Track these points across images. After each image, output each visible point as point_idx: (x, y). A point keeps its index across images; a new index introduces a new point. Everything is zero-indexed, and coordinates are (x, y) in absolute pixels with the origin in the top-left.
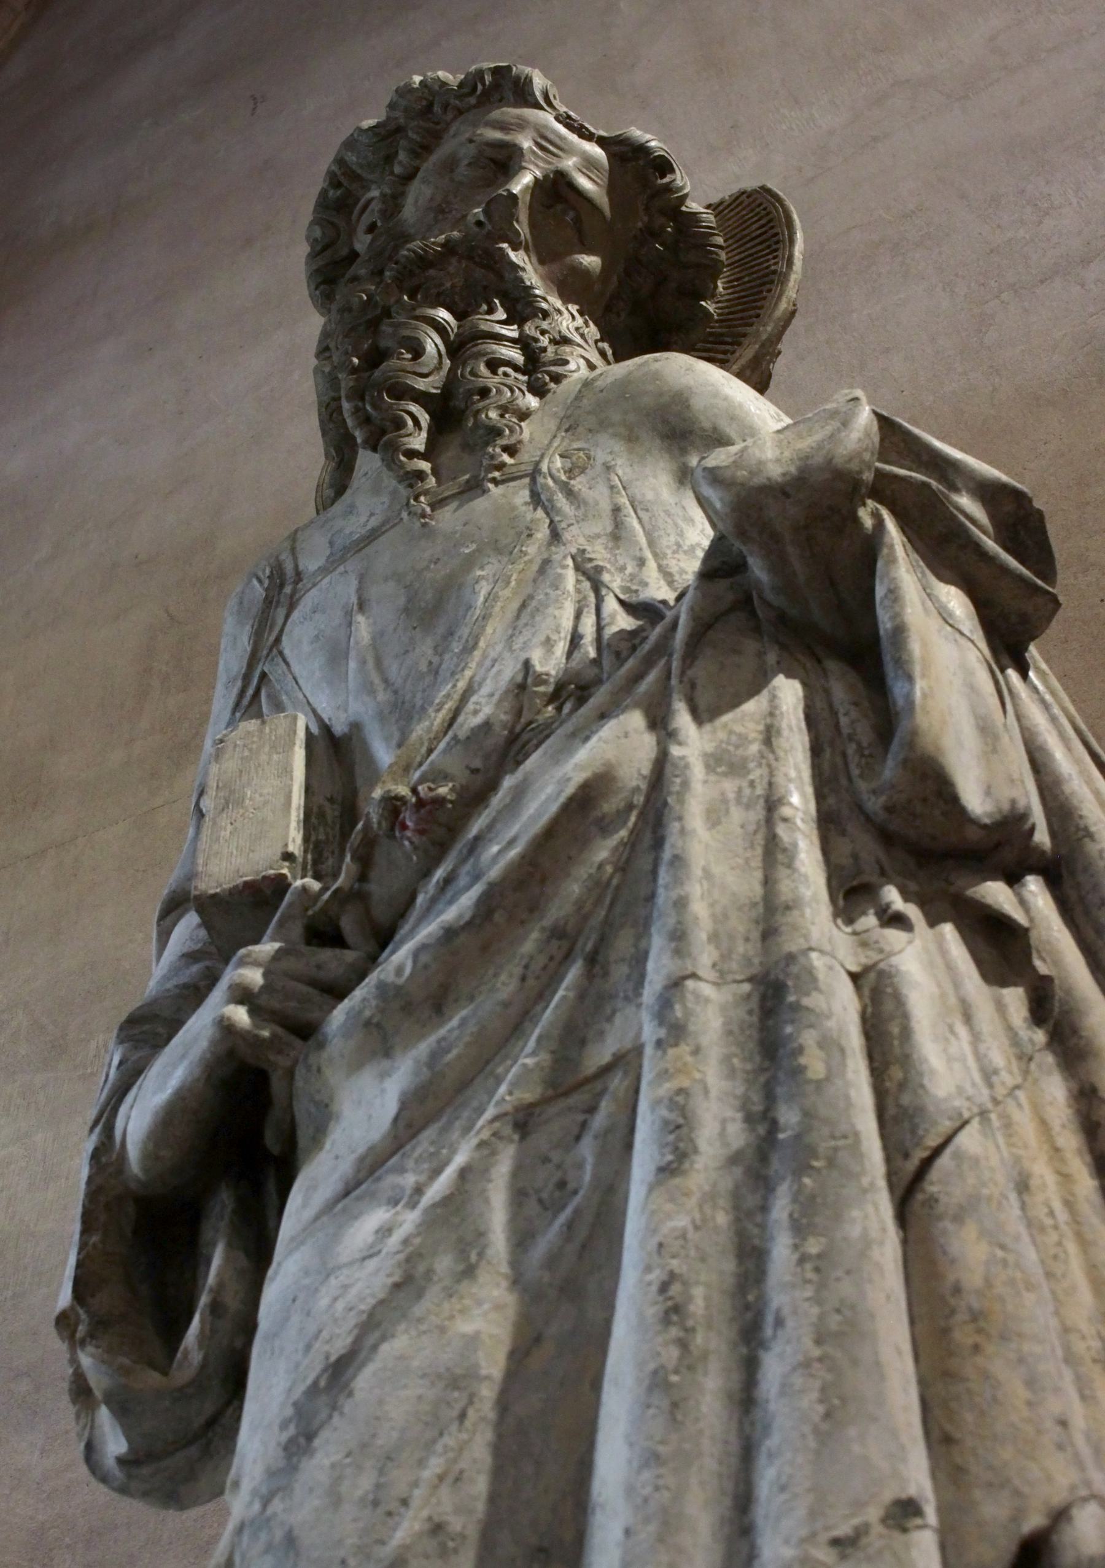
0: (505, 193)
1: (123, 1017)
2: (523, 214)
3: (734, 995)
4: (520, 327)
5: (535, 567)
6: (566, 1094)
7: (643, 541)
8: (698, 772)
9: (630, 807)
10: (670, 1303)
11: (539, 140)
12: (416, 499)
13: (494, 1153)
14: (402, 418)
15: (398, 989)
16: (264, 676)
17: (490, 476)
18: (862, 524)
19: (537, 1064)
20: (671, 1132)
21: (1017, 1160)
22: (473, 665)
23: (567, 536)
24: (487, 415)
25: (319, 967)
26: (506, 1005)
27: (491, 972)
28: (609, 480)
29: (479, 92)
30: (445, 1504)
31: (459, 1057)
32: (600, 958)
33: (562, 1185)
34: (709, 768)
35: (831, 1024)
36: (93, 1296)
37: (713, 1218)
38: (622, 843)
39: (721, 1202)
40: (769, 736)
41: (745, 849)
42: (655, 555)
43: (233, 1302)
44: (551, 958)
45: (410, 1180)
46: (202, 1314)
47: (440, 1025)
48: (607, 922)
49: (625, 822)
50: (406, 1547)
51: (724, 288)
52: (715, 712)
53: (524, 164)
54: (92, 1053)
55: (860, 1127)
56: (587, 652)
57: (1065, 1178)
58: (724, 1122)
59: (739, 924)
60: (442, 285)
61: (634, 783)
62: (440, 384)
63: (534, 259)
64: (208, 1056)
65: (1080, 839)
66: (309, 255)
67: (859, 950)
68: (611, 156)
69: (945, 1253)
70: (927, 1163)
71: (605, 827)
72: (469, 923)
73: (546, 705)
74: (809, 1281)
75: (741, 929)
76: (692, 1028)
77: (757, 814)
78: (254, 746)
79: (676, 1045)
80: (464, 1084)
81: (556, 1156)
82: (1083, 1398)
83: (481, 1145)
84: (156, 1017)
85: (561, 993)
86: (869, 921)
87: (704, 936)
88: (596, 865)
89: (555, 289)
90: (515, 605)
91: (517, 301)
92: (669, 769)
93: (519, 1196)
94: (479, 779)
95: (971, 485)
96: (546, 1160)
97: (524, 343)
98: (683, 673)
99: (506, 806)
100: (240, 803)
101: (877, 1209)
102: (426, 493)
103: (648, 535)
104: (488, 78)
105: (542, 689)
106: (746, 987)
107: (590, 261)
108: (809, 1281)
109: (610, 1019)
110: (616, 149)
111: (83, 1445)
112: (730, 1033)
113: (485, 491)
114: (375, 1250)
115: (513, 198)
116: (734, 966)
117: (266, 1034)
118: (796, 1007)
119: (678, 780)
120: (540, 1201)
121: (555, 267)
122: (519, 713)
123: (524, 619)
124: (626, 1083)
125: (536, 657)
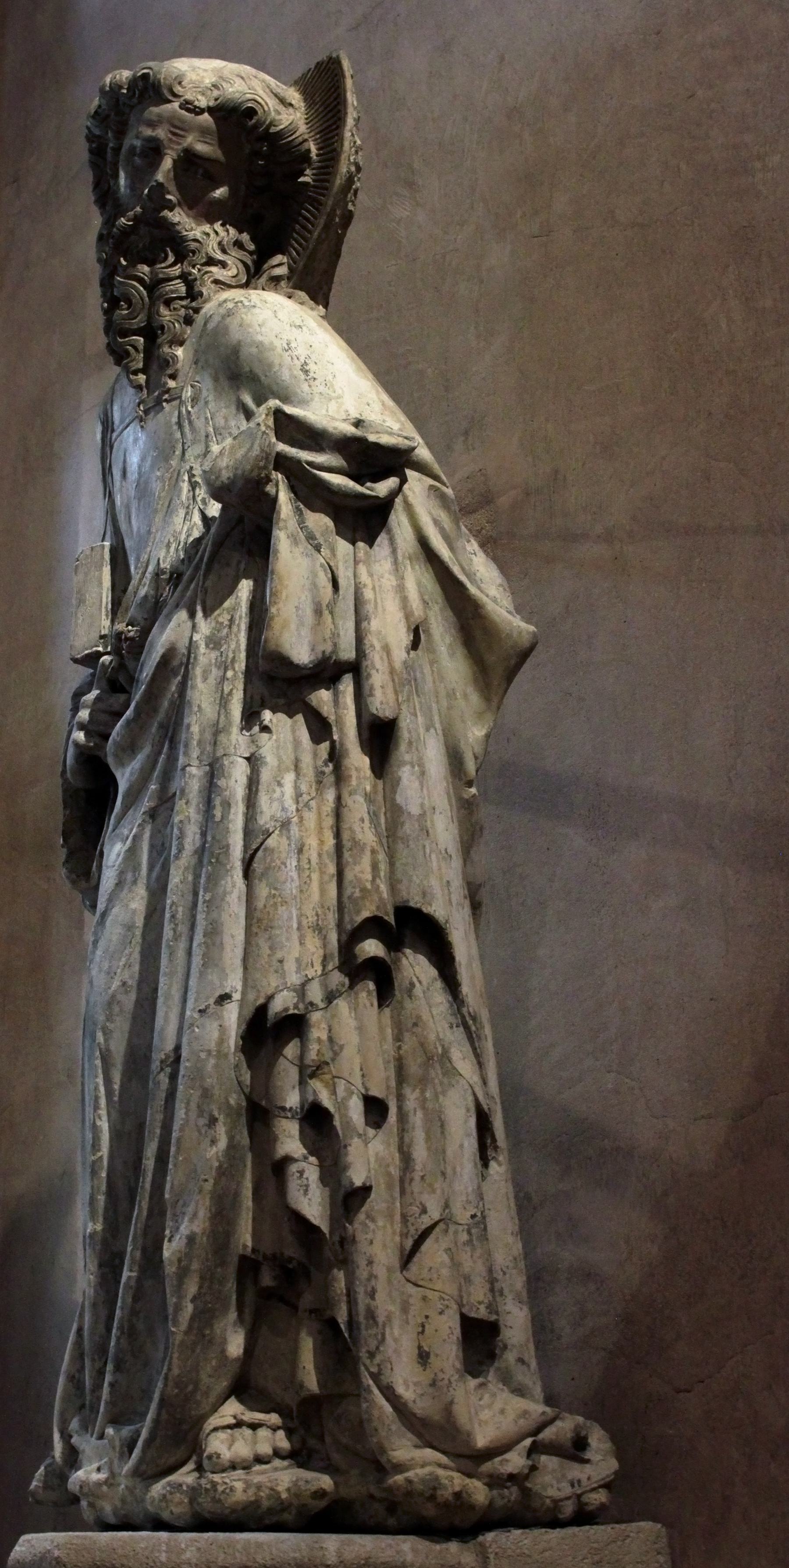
0: (154, 184)
1: (71, 695)
2: (172, 187)
4: (182, 265)
8: (202, 649)
9: (181, 664)
11: (172, 129)
13: (143, 829)
21: (301, 837)
22: (150, 544)
23: (187, 456)
25: (111, 706)
30: (126, 975)
33: (163, 844)
34: (207, 646)
35: (227, 793)
39: (191, 871)
50: (115, 991)
51: (317, 155)
52: (213, 610)
57: (322, 842)
58: (195, 834)
59: (208, 736)
62: (145, 318)
63: (186, 208)
76: (187, 791)
82: (301, 944)
86: (256, 729)
87: (195, 743)
89: (203, 219)
93: (152, 847)
97: (184, 277)
98: (204, 583)
104: (140, 84)
106: (208, 768)
107: (220, 192)
113: (163, 408)
115: (160, 185)
117: (92, 744)
125: (162, 554)
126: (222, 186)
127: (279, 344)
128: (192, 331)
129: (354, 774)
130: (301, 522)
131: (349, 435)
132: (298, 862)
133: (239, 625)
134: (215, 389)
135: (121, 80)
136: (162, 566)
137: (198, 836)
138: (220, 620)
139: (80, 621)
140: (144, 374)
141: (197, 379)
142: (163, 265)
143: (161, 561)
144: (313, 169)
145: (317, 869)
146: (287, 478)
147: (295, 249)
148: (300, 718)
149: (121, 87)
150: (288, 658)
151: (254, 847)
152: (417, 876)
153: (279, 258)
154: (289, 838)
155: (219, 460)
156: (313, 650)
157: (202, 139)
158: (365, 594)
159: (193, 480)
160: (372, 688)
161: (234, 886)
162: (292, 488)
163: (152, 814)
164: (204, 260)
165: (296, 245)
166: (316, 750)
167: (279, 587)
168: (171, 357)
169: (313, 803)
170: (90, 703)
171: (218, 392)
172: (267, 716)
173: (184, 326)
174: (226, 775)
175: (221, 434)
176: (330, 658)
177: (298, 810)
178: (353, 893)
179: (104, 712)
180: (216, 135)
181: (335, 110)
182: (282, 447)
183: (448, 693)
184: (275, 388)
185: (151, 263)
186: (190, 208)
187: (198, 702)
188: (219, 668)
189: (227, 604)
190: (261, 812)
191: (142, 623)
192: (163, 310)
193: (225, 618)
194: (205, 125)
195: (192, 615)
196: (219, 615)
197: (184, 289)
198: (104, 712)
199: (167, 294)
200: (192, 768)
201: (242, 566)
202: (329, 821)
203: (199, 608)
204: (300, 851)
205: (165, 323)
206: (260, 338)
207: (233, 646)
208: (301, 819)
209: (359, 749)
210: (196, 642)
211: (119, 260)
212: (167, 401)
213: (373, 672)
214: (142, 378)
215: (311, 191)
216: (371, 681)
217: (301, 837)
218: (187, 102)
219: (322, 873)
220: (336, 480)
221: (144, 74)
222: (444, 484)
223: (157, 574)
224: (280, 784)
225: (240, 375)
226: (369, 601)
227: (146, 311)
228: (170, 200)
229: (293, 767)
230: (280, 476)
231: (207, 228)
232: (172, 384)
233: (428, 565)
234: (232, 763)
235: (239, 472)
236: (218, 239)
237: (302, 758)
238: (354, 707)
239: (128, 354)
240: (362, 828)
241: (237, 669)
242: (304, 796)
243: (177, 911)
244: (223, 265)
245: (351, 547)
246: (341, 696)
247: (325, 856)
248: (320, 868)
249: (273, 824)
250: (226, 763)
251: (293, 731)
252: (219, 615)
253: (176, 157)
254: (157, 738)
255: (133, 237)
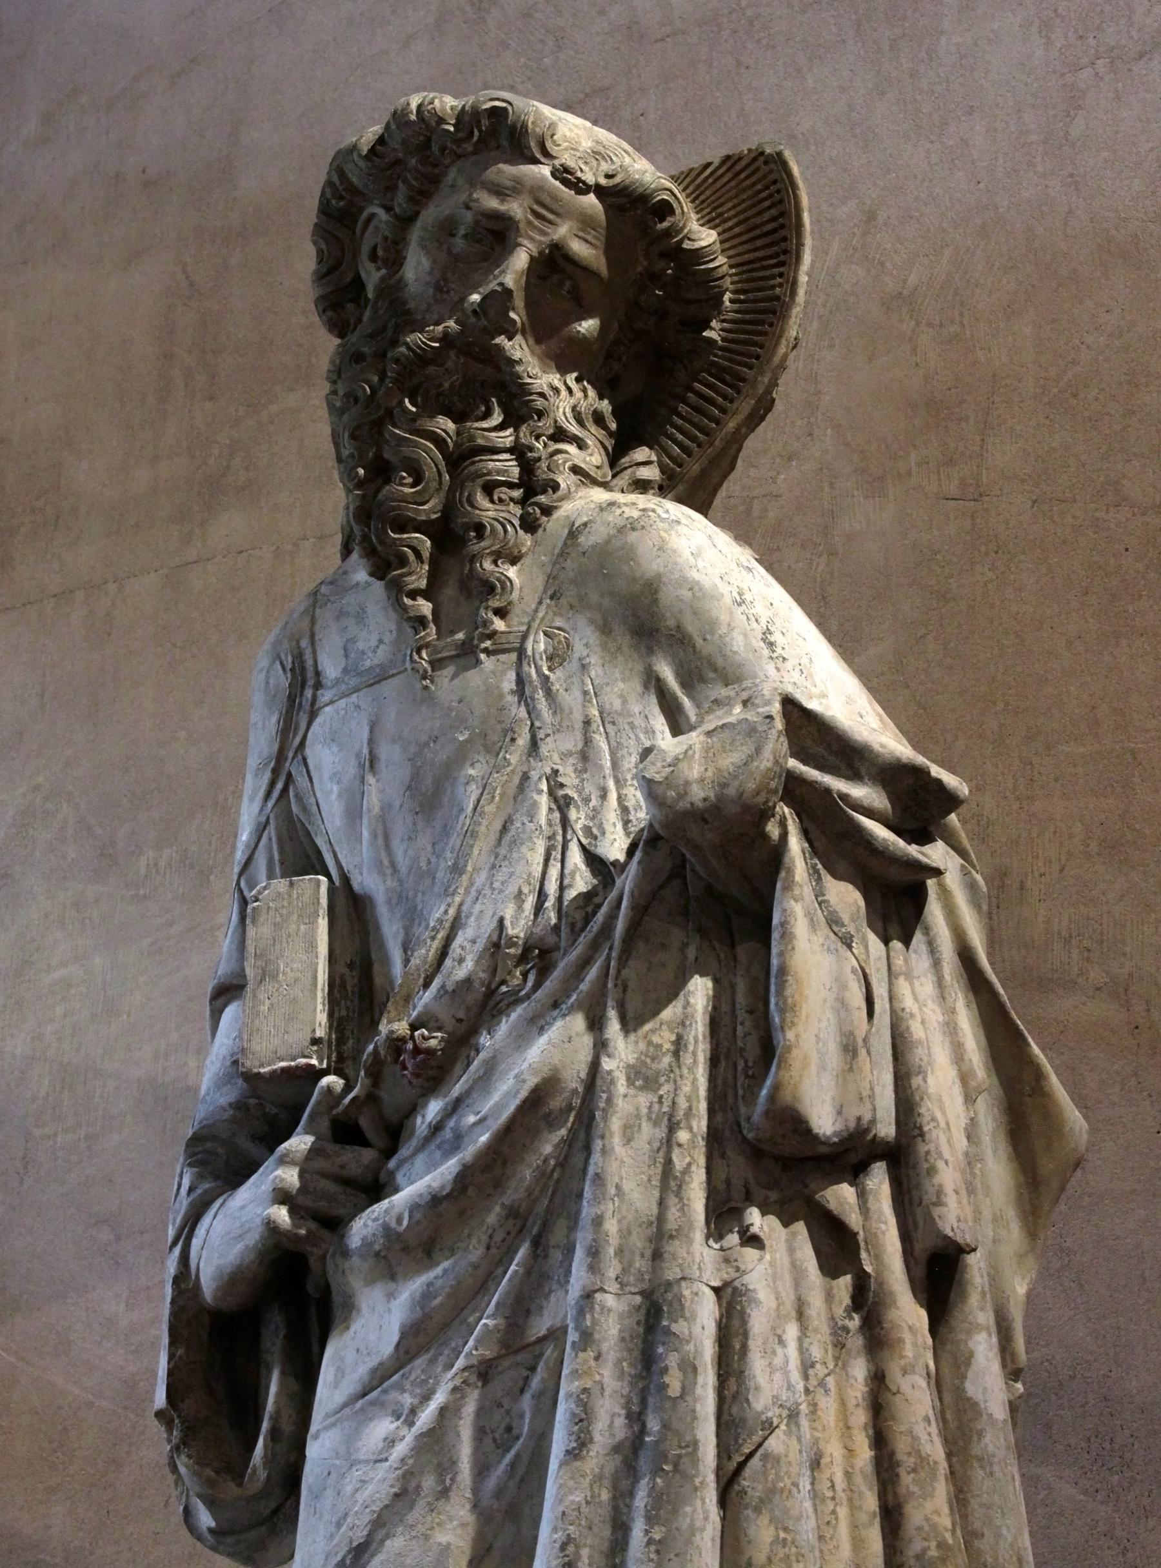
0: (499, 289)
2: (519, 301)
3: (629, 1304)
4: (516, 430)
5: (516, 780)
6: (517, 1352)
7: (608, 770)
8: (621, 1086)
9: (570, 1108)
10: (567, 1559)
11: (535, 207)
12: (419, 652)
13: (463, 1397)
14: (405, 553)
15: (399, 1236)
16: (289, 776)
17: (483, 645)
18: (770, 838)
19: (495, 1326)
20: (577, 1424)
21: (817, 1441)
22: (461, 891)
23: (544, 749)
24: (481, 566)
25: (343, 1167)
26: (476, 1267)
27: (466, 1232)
28: (583, 683)
29: (475, 139)
31: (441, 1305)
32: (543, 1241)
33: (509, 1429)
34: (630, 1082)
35: (690, 1348)
36: (183, 1401)
37: (599, 1495)
38: (563, 1140)
39: (606, 1483)
40: (679, 1045)
41: (649, 1166)
42: (617, 781)
43: (287, 1427)
44: (509, 1233)
45: (408, 1400)
46: (265, 1440)
47: (429, 1267)
48: (549, 1211)
49: (566, 1121)
52: (641, 1021)
53: (520, 240)
54: (143, 871)
55: (700, 1435)
56: (550, 919)
57: (850, 1452)
58: (613, 1415)
59: (638, 1241)
60: (441, 385)
61: (574, 1085)
62: (440, 507)
63: (531, 341)
64: (260, 1246)
65: (914, 1137)
66: (316, 272)
67: (723, 1266)
68: (608, 208)
69: (746, 1535)
70: (742, 1465)
71: (552, 1121)
72: (448, 1195)
73: (516, 967)
74: (651, 1560)
75: (639, 1245)
76: (597, 1336)
77: (661, 1133)
78: (284, 911)
79: (585, 1350)
80: (445, 1326)
81: (506, 1402)
83: (455, 1389)
84: (214, 1138)
85: (513, 1267)
86: (733, 1239)
87: (611, 1251)
88: (542, 1158)
90: (497, 825)
91: (514, 396)
92: (599, 1082)
93: (480, 1433)
94: (463, 1028)
95: (874, 771)
96: (500, 1405)
97: (519, 451)
98: (619, 971)
99: (480, 1078)
100: (274, 976)
101: (703, 1502)
102: (427, 646)
103: (613, 753)
104: (485, 123)
105: (512, 951)
106: (638, 1299)
107: (588, 326)
108: (651, 1560)
109: (547, 1297)
110: (612, 200)
111: (182, 1508)
112: (623, 1339)
113: (478, 662)
114: (384, 1456)
115: (507, 293)
116: (632, 1279)
117: (303, 1232)
118: (668, 1332)
119: (604, 1096)
120: (495, 1440)
121: (553, 344)
122: (494, 972)
123: (503, 851)
124: (555, 1355)
125: (509, 912)
126: (592, 318)
127: (727, 592)
128: (536, 543)
129: (907, 1337)
130: (819, 893)
131: (905, 760)
132: (812, 1484)
133: (694, 1054)
134: (604, 647)
135: (443, 109)
136: (511, 932)
137: (620, 1422)
138: (656, 1039)
139: (264, 1008)
140: (428, 600)
141: (558, 624)
142: (485, 425)
143: (507, 923)
144: (723, 321)
145: (845, 1503)
146: (798, 815)
147: (675, 441)
148: (800, 1227)
149: (441, 120)
150: (807, 1122)
151: (747, 1451)
152: (1008, 1528)
153: (641, 453)
154: (799, 1439)
155: (683, 766)
156: (839, 1113)
157: (581, 234)
158: (913, 1029)
159: (561, 793)
160: (940, 1192)
161: (706, 1518)
162: (806, 834)
163: (484, 1372)
164: (551, 431)
165: (680, 437)
166: (831, 1288)
167: (797, 997)
168: (499, 580)
169: (830, 1380)
170: (299, 1156)
171: (611, 654)
172: (755, 1218)
173: (521, 532)
174: (688, 1314)
175: (613, 723)
176: (867, 1131)
177: (807, 1391)
178: (925, 1550)
179: (325, 1175)
180: (603, 232)
181: (777, 236)
182: (792, 763)
183: (994, 1214)
184: (720, 662)
185: (458, 418)
186: (538, 341)
187: (616, 1180)
188: (656, 1124)
189: (667, 1014)
190: (757, 1388)
191: (450, 1024)
192: (481, 499)
193: (665, 1039)
194: (589, 212)
195: (596, 1024)
196: (653, 1031)
197: (516, 471)
198: (325, 1175)
199: (489, 473)
200: (608, 1296)
201: (691, 953)
202: (860, 1417)
203: (612, 1014)
204: (816, 1464)
205: (485, 521)
206: (695, 575)
207: (686, 1089)
208: (814, 1407)
209: (911, 1295)
210: (610, 1072)
211: (402, 402)
212: (486, 651)
213: (940, 1165)
214: (425, 607)
215: (716, 356)
216: (936, 1180)
217: (817, 1441)
218: (566, 170)
219: (853, 1507)
220: (880, 832)
221: (494, 109)
222: (974, 867)
223: (497, 945)
224: (781, 1342)
225: (657, 630)
226: (920, 1042)
227: (443, 494)
228: (514, 321)
229: (794, 1314)
230: (786, 810)
231: (555, 379)
232: (499, 625)
233: (971, 996)
234: (696, 1294)
235: (731, 791)
236: (573, 401)
237: (811, 1299)
238: (894, 1220)
239: (403, 561)
240: (929, 1434)
241: (695, 1129)
242: (818, 1366)
243: (578, 1556)
244: (581, 445)
245: (882, 946)
246: (871, 1199)
247: (859, 1480)
248: (850, 1500)
249: (777, 1411)
250: (686, 1293)
251: (791, 1250)
252: (653, 1031)
253: (535, 254)
254: (499, 1236)
255: (432, 369)
